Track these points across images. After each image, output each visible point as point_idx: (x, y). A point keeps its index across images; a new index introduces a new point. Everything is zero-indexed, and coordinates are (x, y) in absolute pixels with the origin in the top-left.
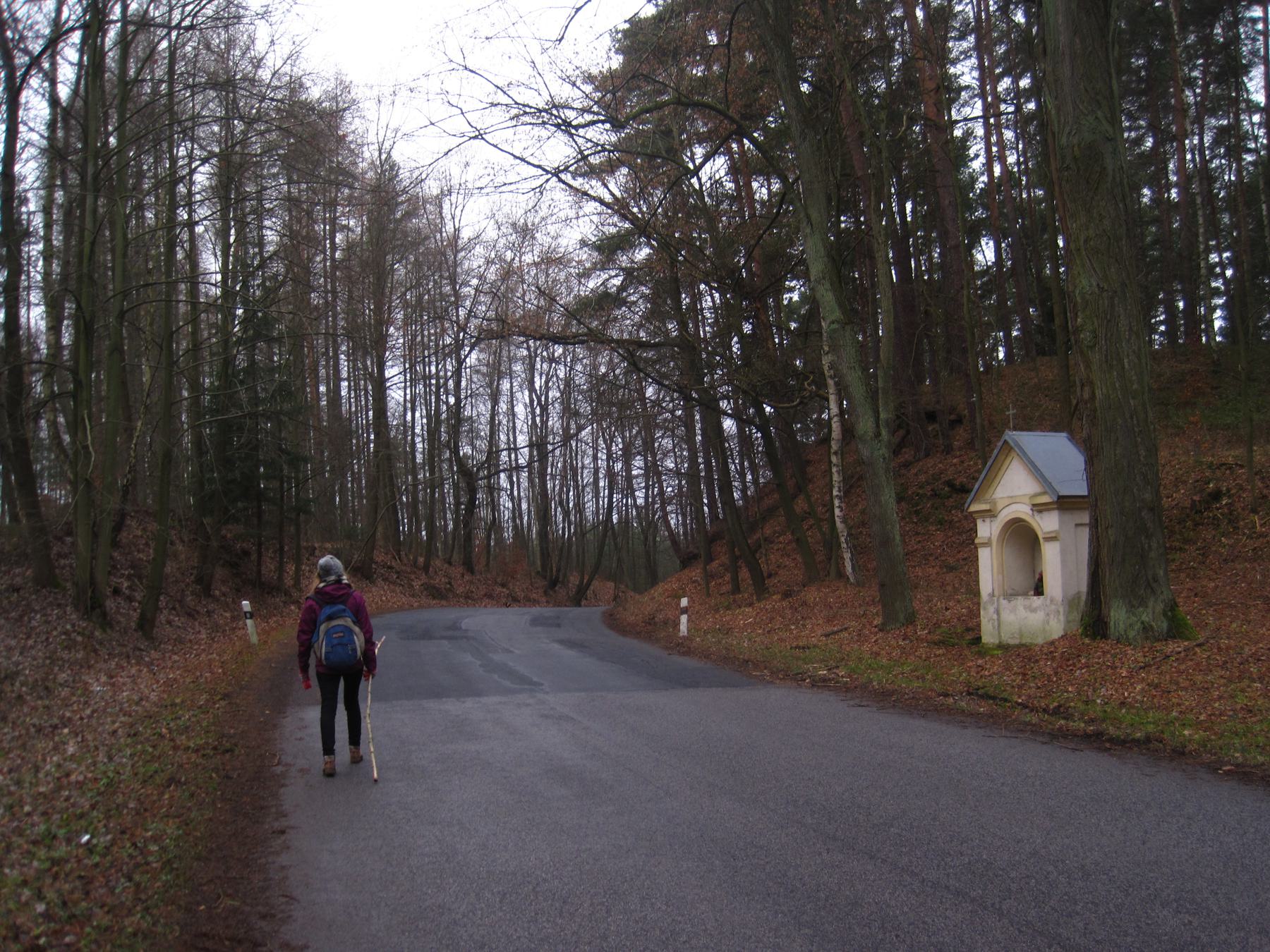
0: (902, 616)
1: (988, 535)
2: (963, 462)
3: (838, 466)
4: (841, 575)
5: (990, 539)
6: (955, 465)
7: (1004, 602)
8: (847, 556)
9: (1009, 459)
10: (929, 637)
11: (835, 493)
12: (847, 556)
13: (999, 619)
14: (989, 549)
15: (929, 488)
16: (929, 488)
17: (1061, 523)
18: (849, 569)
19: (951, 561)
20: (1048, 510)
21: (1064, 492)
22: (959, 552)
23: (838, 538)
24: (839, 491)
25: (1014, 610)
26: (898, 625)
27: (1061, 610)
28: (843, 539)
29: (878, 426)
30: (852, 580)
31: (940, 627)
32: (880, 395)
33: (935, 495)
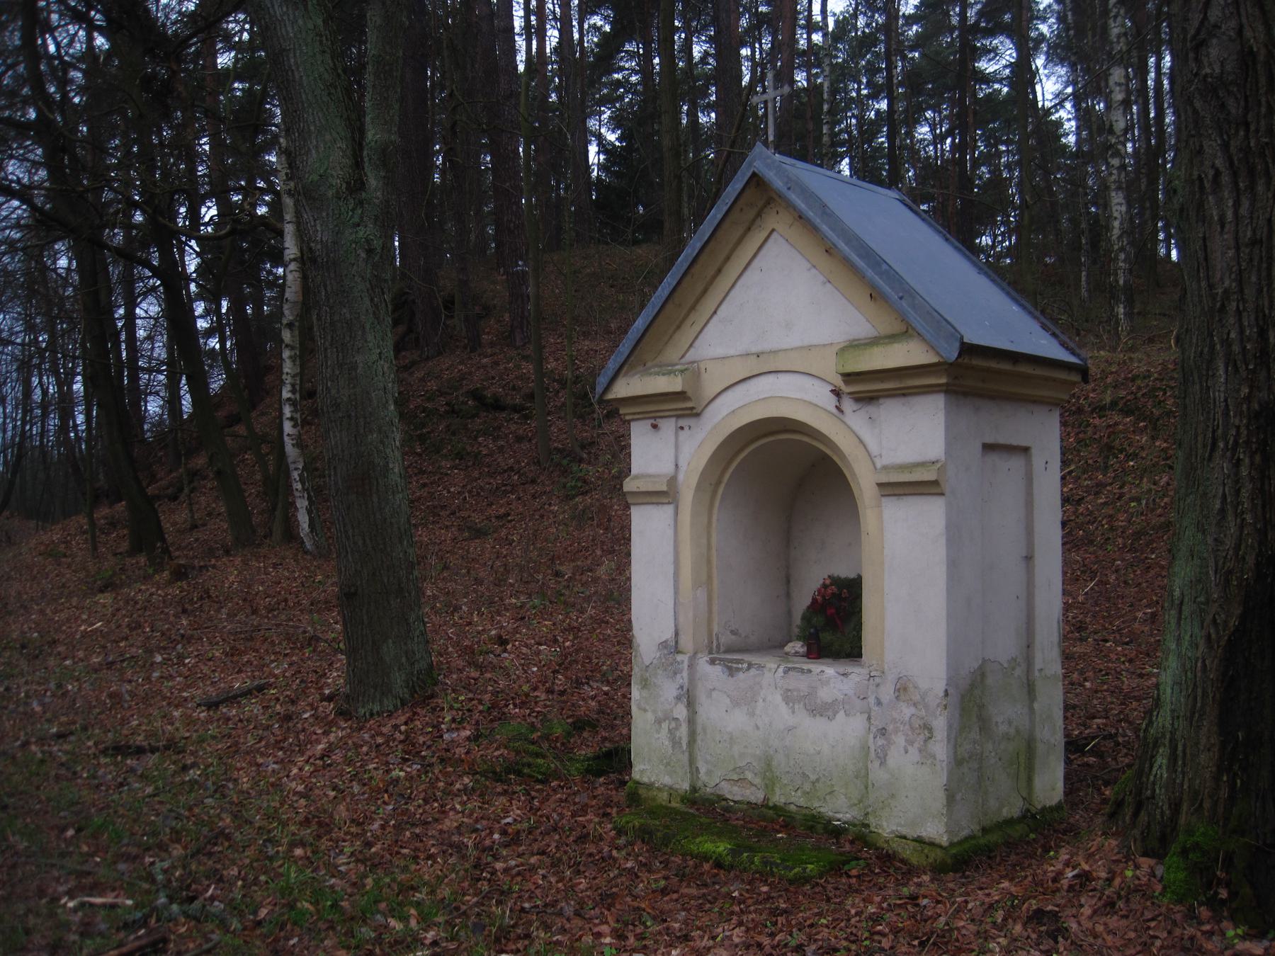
0: (398, 680)
1: (668, 468)
2: (497, 363)
3: (292, 348)
4: (290, 534)
5: (673, 480)
6: (484, 367)
7: (712, 674)
8: (302, 504)
9: (757, 237)
10: (477, 753)
11: (286, 394)
12: (302, 504)
13: (691, 721)
14: (669, 509)
15: (443, 400)
16: (443, 400)
17: (950, 441)
18: (303, 519)
19: (477, 518)
20: (904, 393)
21: (973, 337)
22: (490, 505)
23: (288, 475)
24: (293, 391)
25: (747, 700)
26: (389, 703)
27: (940, 724)
28: (295, 475)
29: (358, 164)
30: (309, 545)
31: (503, 717)
32: (369, 78)
33: (453, 411)
